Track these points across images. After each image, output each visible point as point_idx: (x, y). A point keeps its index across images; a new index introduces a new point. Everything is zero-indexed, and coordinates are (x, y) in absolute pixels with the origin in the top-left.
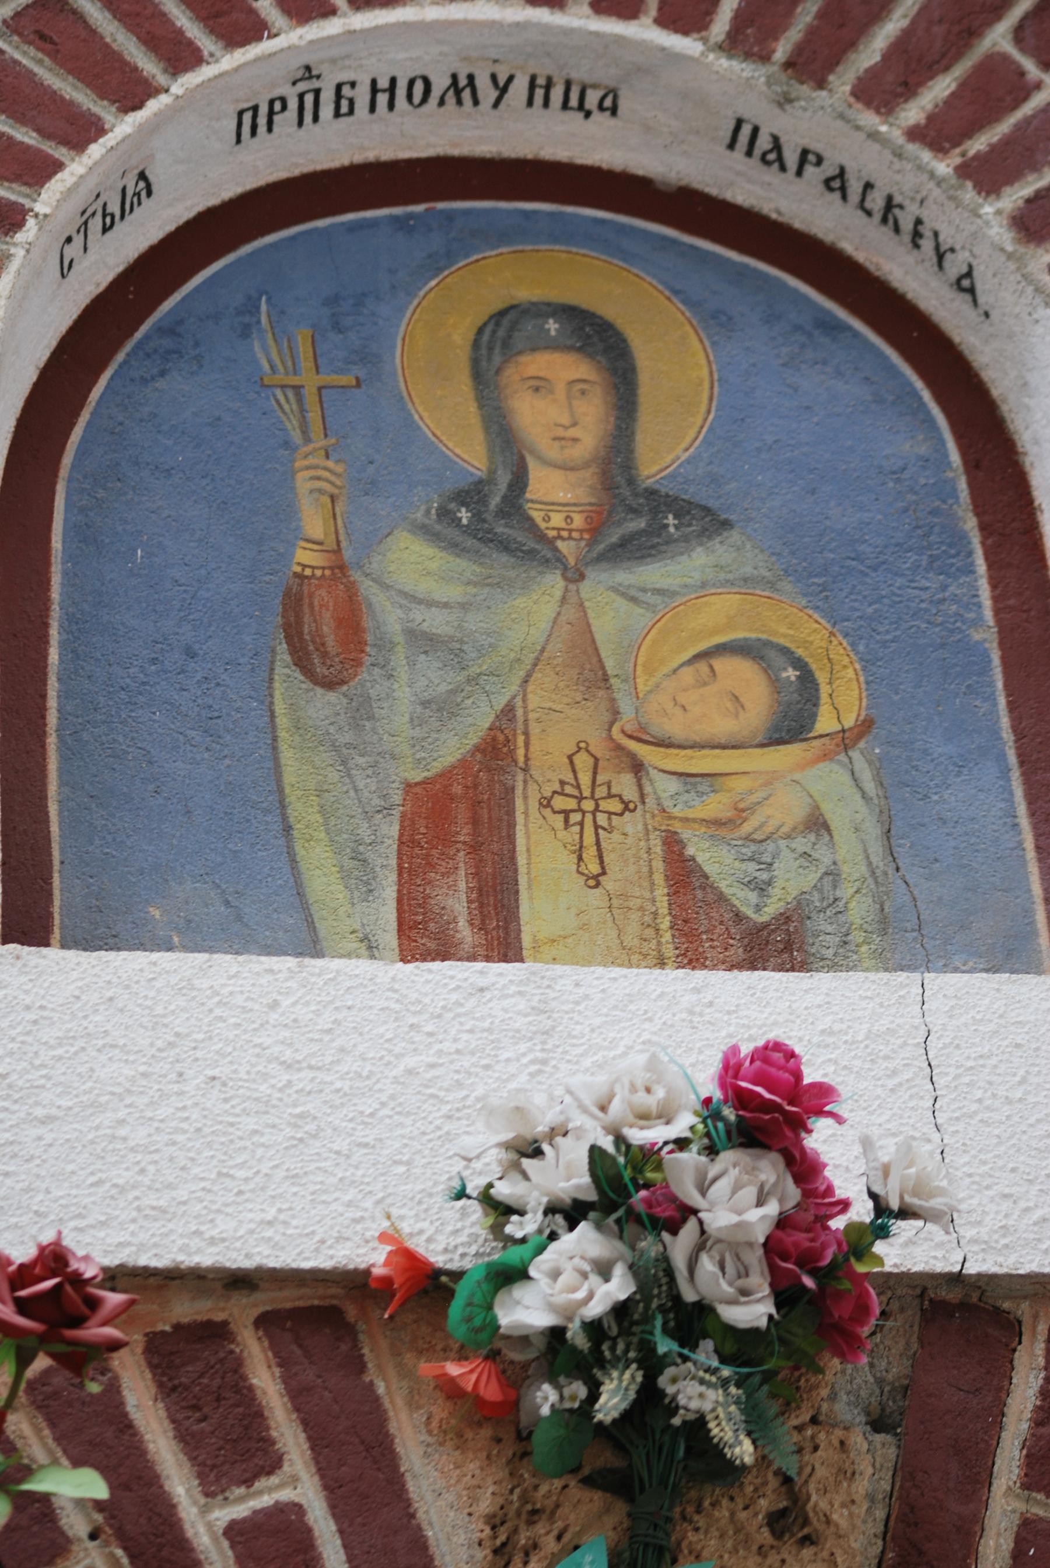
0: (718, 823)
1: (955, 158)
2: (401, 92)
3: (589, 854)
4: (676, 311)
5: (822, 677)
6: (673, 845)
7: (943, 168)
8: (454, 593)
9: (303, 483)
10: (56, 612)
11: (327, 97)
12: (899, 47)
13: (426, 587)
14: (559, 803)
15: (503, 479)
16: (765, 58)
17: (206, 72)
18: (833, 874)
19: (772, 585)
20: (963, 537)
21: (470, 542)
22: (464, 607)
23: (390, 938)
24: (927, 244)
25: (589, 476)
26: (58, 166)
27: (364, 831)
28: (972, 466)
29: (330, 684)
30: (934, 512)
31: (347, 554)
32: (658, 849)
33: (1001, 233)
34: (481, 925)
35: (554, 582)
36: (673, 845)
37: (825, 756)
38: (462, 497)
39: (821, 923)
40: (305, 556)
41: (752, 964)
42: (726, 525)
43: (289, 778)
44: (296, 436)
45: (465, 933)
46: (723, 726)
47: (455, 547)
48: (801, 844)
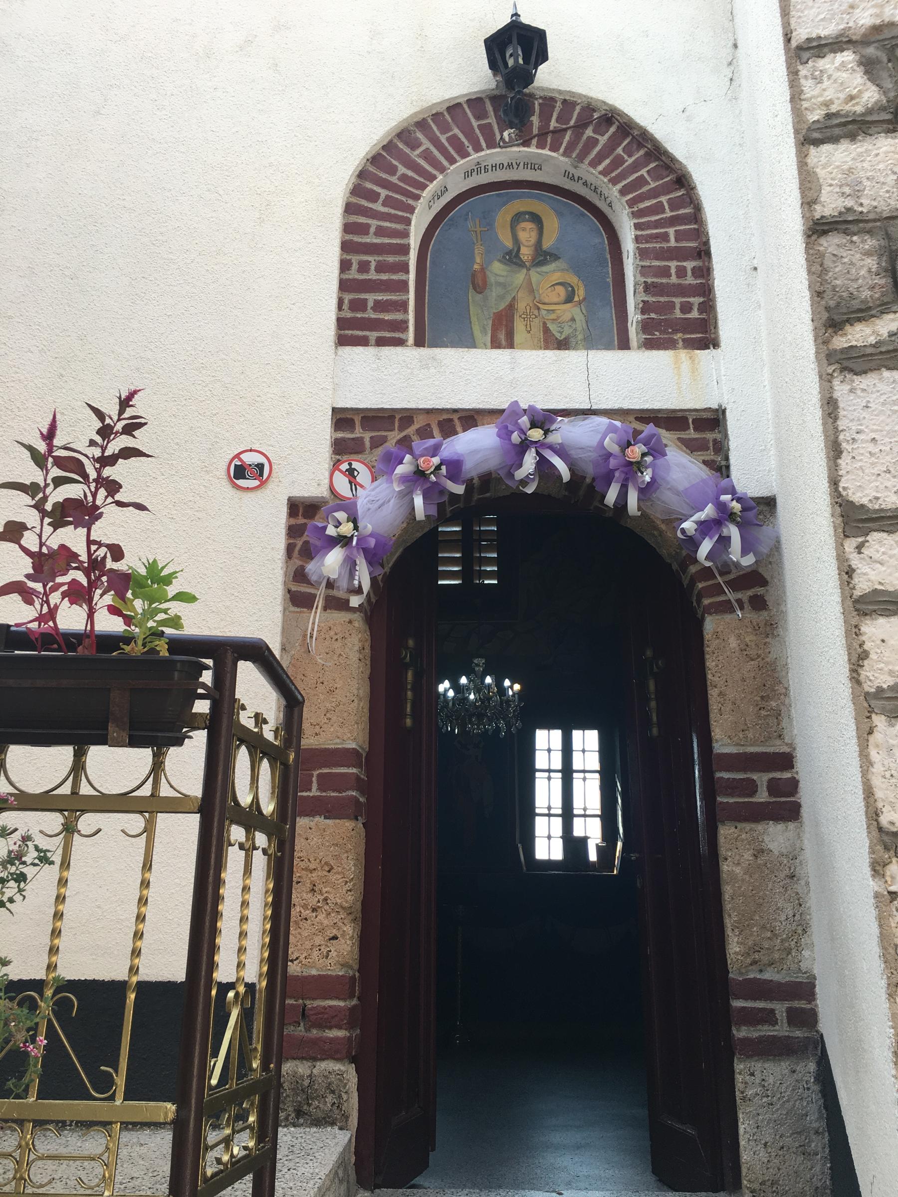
0: (554, 320)
1: (609, 178)
2: (529, 166)
3: (528, 326)
4: (552, 212)
5: (576, 290)
6: (545, 324)
7: (606, 180)
8: (505, 273)
9: (476, 251)
10: (428, 279)
11: (483, 168)
12: (599, 153)
13: (499, 272)
14: (523, 316)
15: (516, 250)
16: (570, 157)
17: (458, 164)
18: (575, 330)
19: (567, 270)
20: (606, 259)
21: (509, 263)
22: (507, 276)
23: (489, 344)
24: (603, 196)
25: (533, 248)
26: (427, 186)
27: (485, 323)
28: (610, 244)
29: (480, 293)
30: (601, 254)
31: (484, 266)
32: (542, 325)
33: (616, 194)
34: (507, 340)
35: (524, 271)
36: (545, 324)
37: (575, 306)
38: (507, 254)
39: (572, 340)
40: (476, 267)
41: (559, 348)
42: (560, 258)
43: (471, 312)
44: (475, 240)
45: (504, 343)
46: (556, 300)
47: (505, 264)
48: (570, 324)
